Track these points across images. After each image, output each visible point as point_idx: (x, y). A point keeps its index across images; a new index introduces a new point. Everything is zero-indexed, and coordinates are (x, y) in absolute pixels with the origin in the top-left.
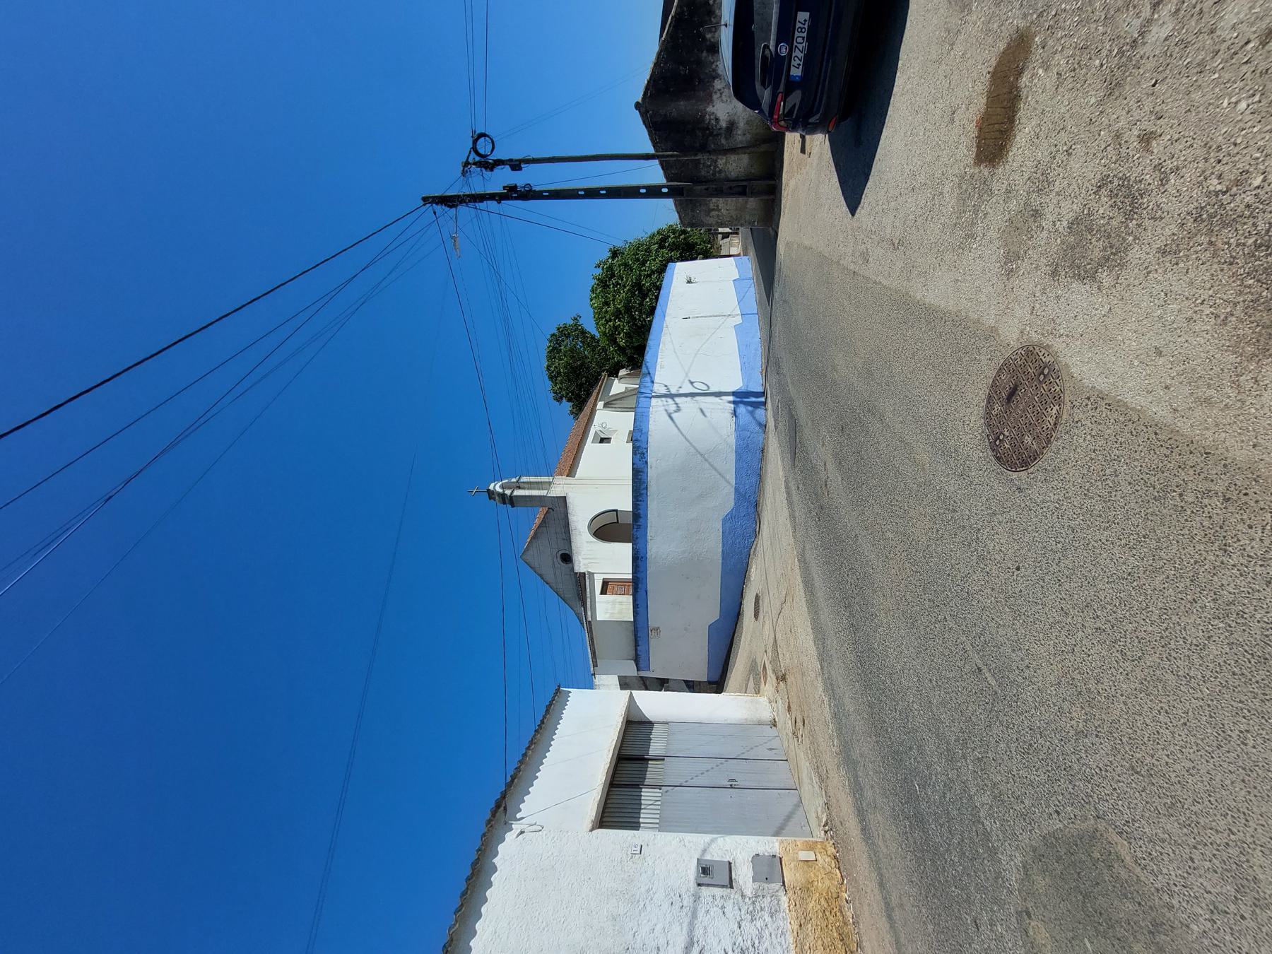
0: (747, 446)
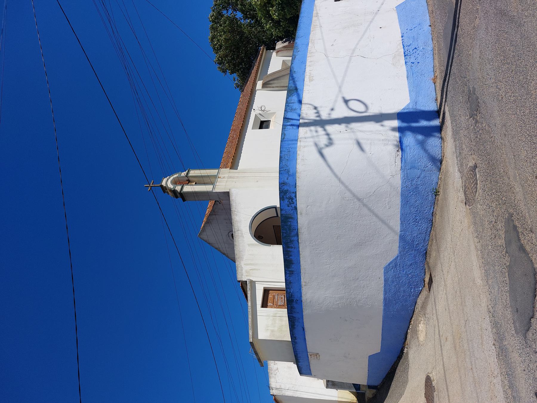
0: (417, 188)
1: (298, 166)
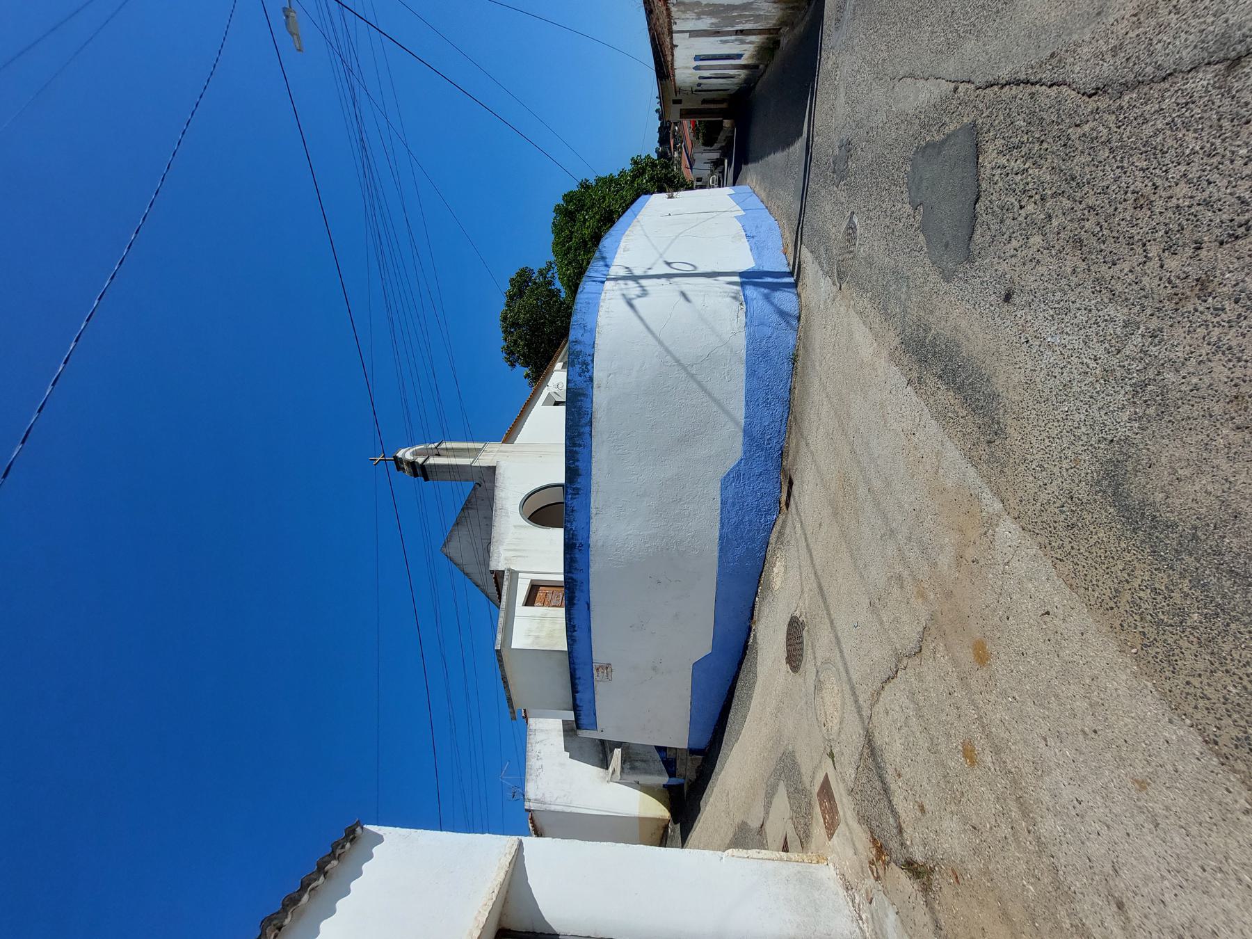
1: (599, 319)
